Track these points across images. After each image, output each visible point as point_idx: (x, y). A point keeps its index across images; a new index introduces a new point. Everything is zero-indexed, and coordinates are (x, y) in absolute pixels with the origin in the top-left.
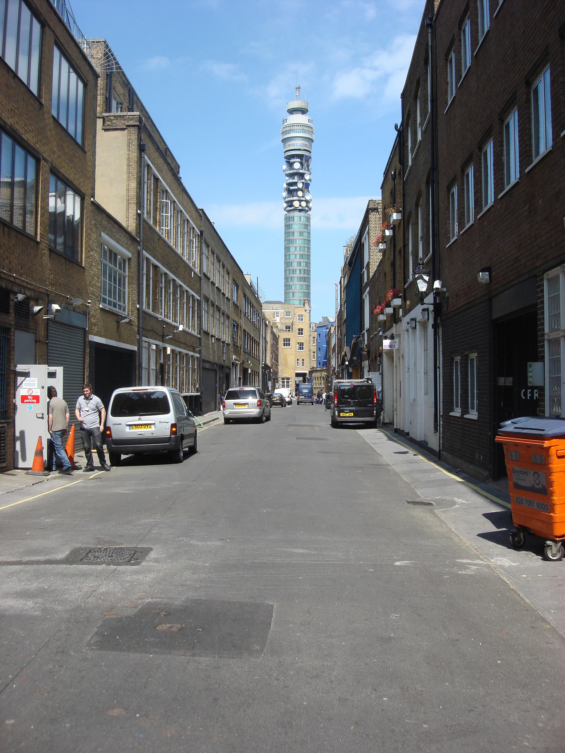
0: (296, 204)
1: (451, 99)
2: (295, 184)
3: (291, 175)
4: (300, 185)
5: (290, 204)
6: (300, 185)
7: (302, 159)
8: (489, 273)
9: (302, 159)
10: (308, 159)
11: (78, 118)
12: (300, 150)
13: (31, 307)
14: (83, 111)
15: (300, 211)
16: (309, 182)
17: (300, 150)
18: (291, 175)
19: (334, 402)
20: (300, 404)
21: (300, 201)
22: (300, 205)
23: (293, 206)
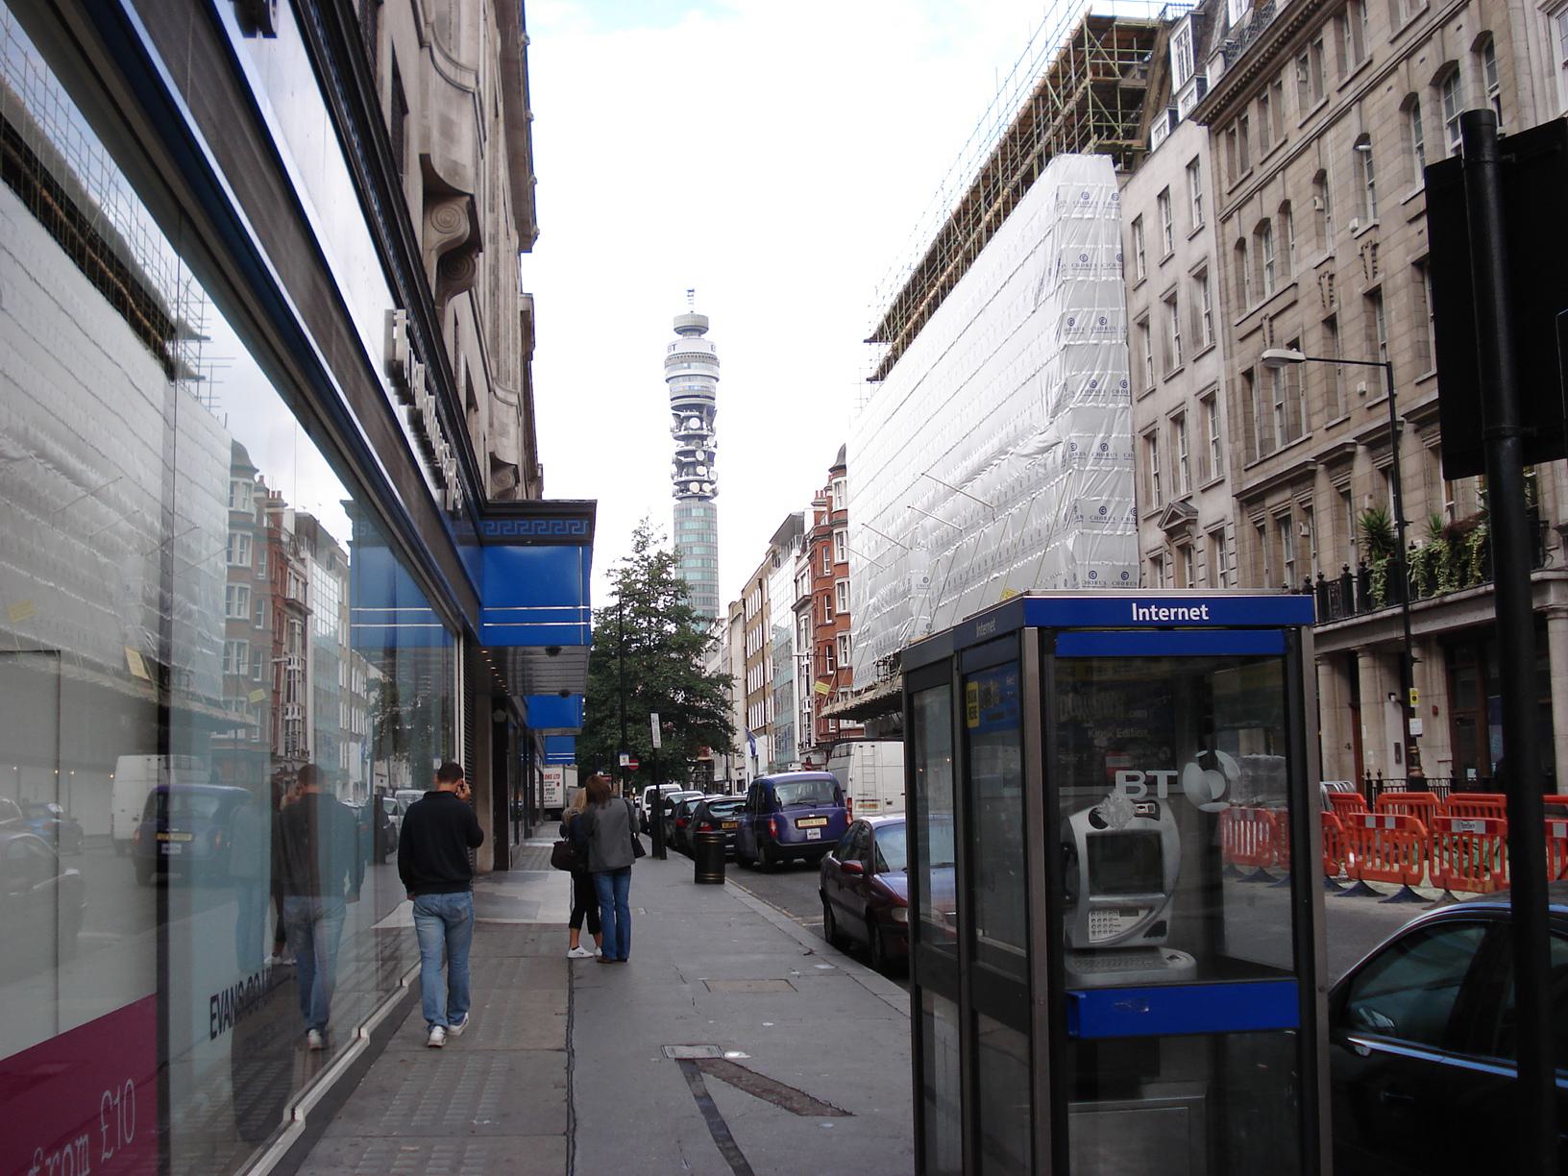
0: (694, 487)
1: (187, 49)
2: (692, 453)
3: (686, 438)
4: (700, 456)
5: (683, 486)
6: (700, 456)
7: (701, 412)
8: (1510, 801)
9: (701, 412)
10: (711, 413)
11: (135, 126)
12: (698, 396)
13: (1556, 508)
14: (410, 573)
15: (702, 498)
16: (714, 450)
17: (698, 396)
18: (686, 438)
19: (1347, 861)
20: (161, 797)
21: (701, 482)
22: (701, 490)
23: (688, 490)
